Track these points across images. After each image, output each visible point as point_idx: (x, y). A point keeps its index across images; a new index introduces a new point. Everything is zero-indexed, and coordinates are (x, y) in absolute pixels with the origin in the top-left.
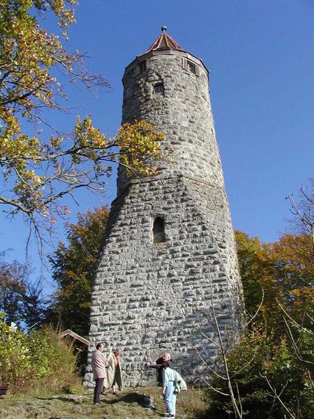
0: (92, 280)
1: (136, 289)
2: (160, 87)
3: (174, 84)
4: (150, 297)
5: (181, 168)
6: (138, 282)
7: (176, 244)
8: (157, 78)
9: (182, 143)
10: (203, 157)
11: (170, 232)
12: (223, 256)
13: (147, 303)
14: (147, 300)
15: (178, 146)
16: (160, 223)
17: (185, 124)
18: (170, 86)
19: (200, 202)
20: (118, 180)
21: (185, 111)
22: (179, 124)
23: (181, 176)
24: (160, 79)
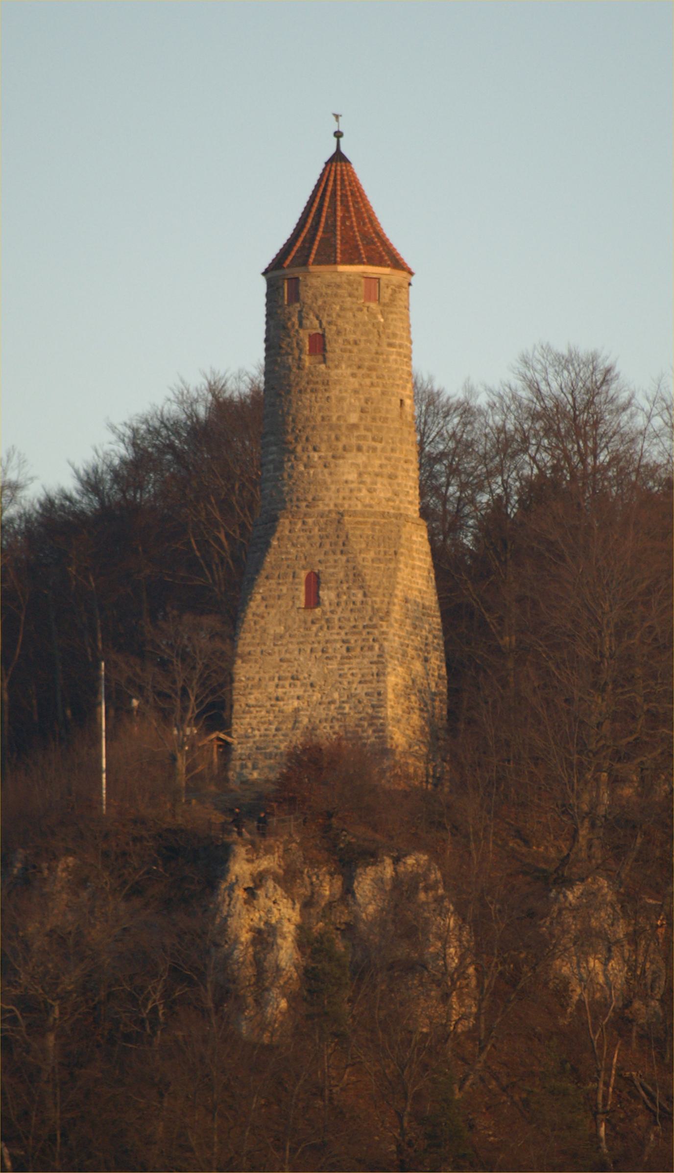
1: (285, 665)
2: (319, 345)
4: (301, 677)
6: (288, 656)
7: (332, 612)
8: (316, 322)
11: (327, 595)
12: (383, 633)
13: (298, 683)
14: (298, 679)
16: (314, 582)
17: (353, 418)
18: (335, 346)
23: (342, 515)
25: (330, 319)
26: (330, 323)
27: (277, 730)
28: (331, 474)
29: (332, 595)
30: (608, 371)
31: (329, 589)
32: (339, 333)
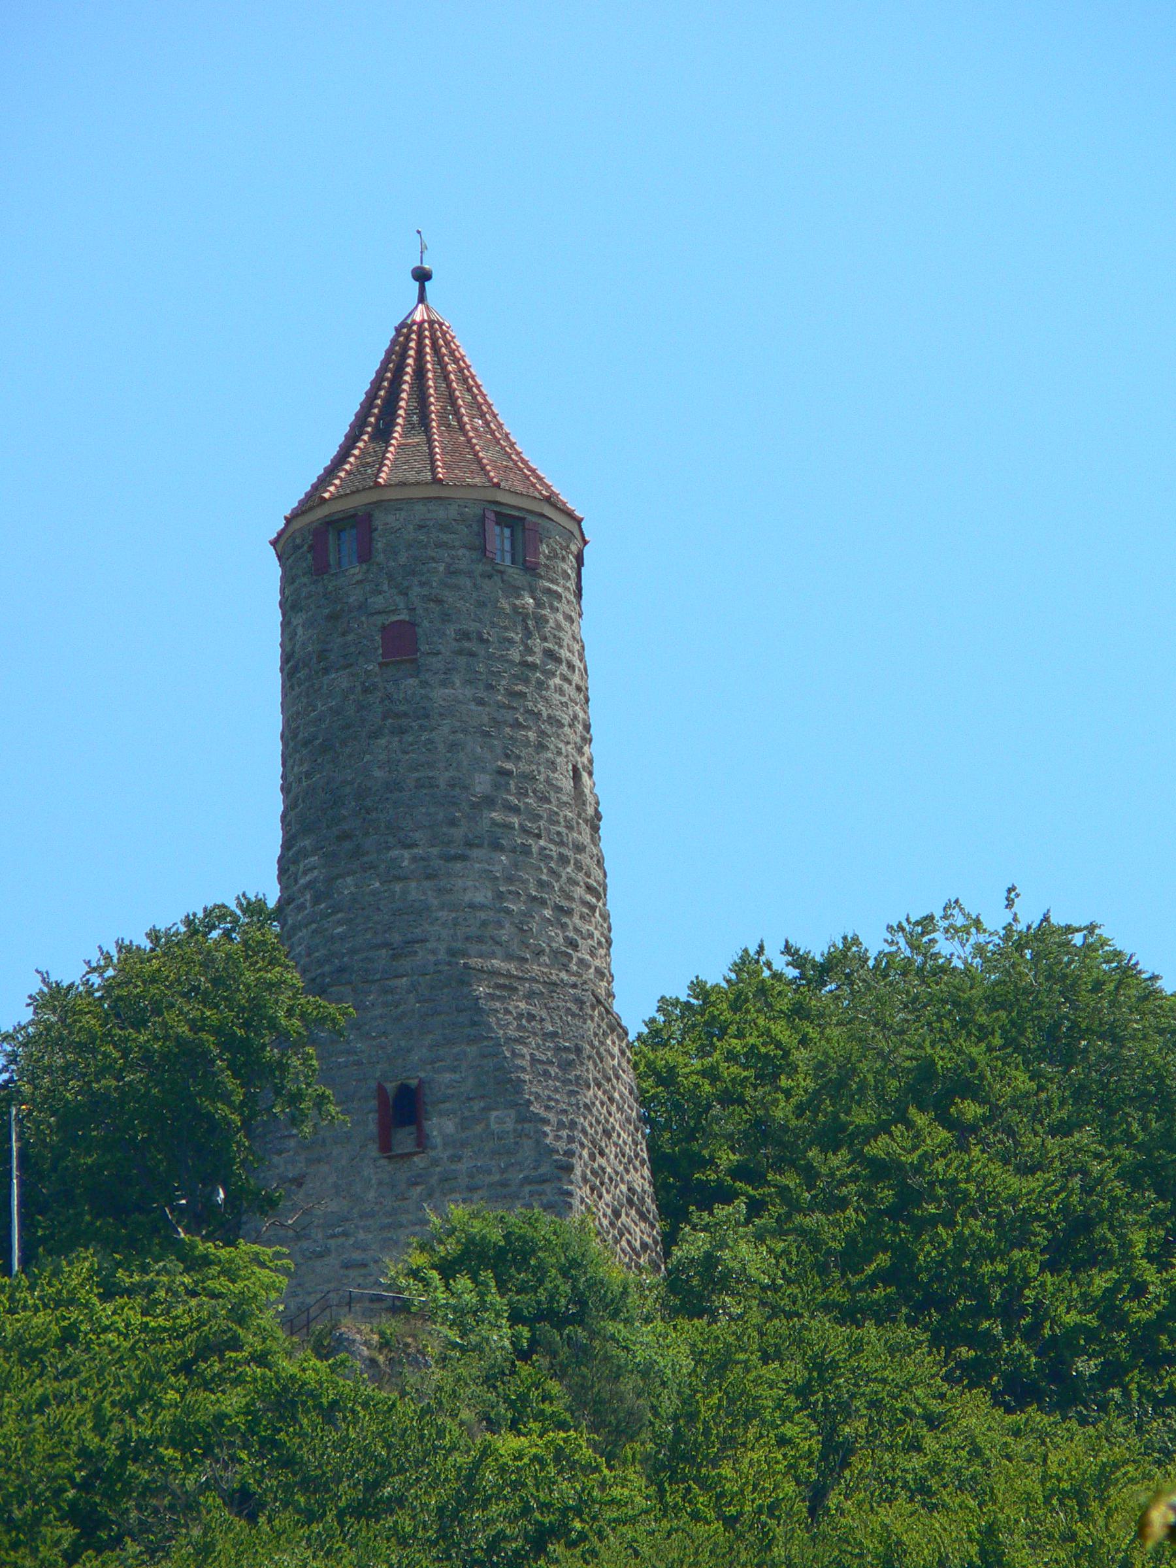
1: (352, 1273)
3: (450, 630)
5: (467, 939)
6: (357, 1256)
9: (475, 853)
15: (459, 866)
25: (425, 591)
26: (428, 599)
27: (460, 1011)
28: (440, 891)
29: (450, 1126)
30: (890, 928)
31: (441, 1114)
32: (446, 617)
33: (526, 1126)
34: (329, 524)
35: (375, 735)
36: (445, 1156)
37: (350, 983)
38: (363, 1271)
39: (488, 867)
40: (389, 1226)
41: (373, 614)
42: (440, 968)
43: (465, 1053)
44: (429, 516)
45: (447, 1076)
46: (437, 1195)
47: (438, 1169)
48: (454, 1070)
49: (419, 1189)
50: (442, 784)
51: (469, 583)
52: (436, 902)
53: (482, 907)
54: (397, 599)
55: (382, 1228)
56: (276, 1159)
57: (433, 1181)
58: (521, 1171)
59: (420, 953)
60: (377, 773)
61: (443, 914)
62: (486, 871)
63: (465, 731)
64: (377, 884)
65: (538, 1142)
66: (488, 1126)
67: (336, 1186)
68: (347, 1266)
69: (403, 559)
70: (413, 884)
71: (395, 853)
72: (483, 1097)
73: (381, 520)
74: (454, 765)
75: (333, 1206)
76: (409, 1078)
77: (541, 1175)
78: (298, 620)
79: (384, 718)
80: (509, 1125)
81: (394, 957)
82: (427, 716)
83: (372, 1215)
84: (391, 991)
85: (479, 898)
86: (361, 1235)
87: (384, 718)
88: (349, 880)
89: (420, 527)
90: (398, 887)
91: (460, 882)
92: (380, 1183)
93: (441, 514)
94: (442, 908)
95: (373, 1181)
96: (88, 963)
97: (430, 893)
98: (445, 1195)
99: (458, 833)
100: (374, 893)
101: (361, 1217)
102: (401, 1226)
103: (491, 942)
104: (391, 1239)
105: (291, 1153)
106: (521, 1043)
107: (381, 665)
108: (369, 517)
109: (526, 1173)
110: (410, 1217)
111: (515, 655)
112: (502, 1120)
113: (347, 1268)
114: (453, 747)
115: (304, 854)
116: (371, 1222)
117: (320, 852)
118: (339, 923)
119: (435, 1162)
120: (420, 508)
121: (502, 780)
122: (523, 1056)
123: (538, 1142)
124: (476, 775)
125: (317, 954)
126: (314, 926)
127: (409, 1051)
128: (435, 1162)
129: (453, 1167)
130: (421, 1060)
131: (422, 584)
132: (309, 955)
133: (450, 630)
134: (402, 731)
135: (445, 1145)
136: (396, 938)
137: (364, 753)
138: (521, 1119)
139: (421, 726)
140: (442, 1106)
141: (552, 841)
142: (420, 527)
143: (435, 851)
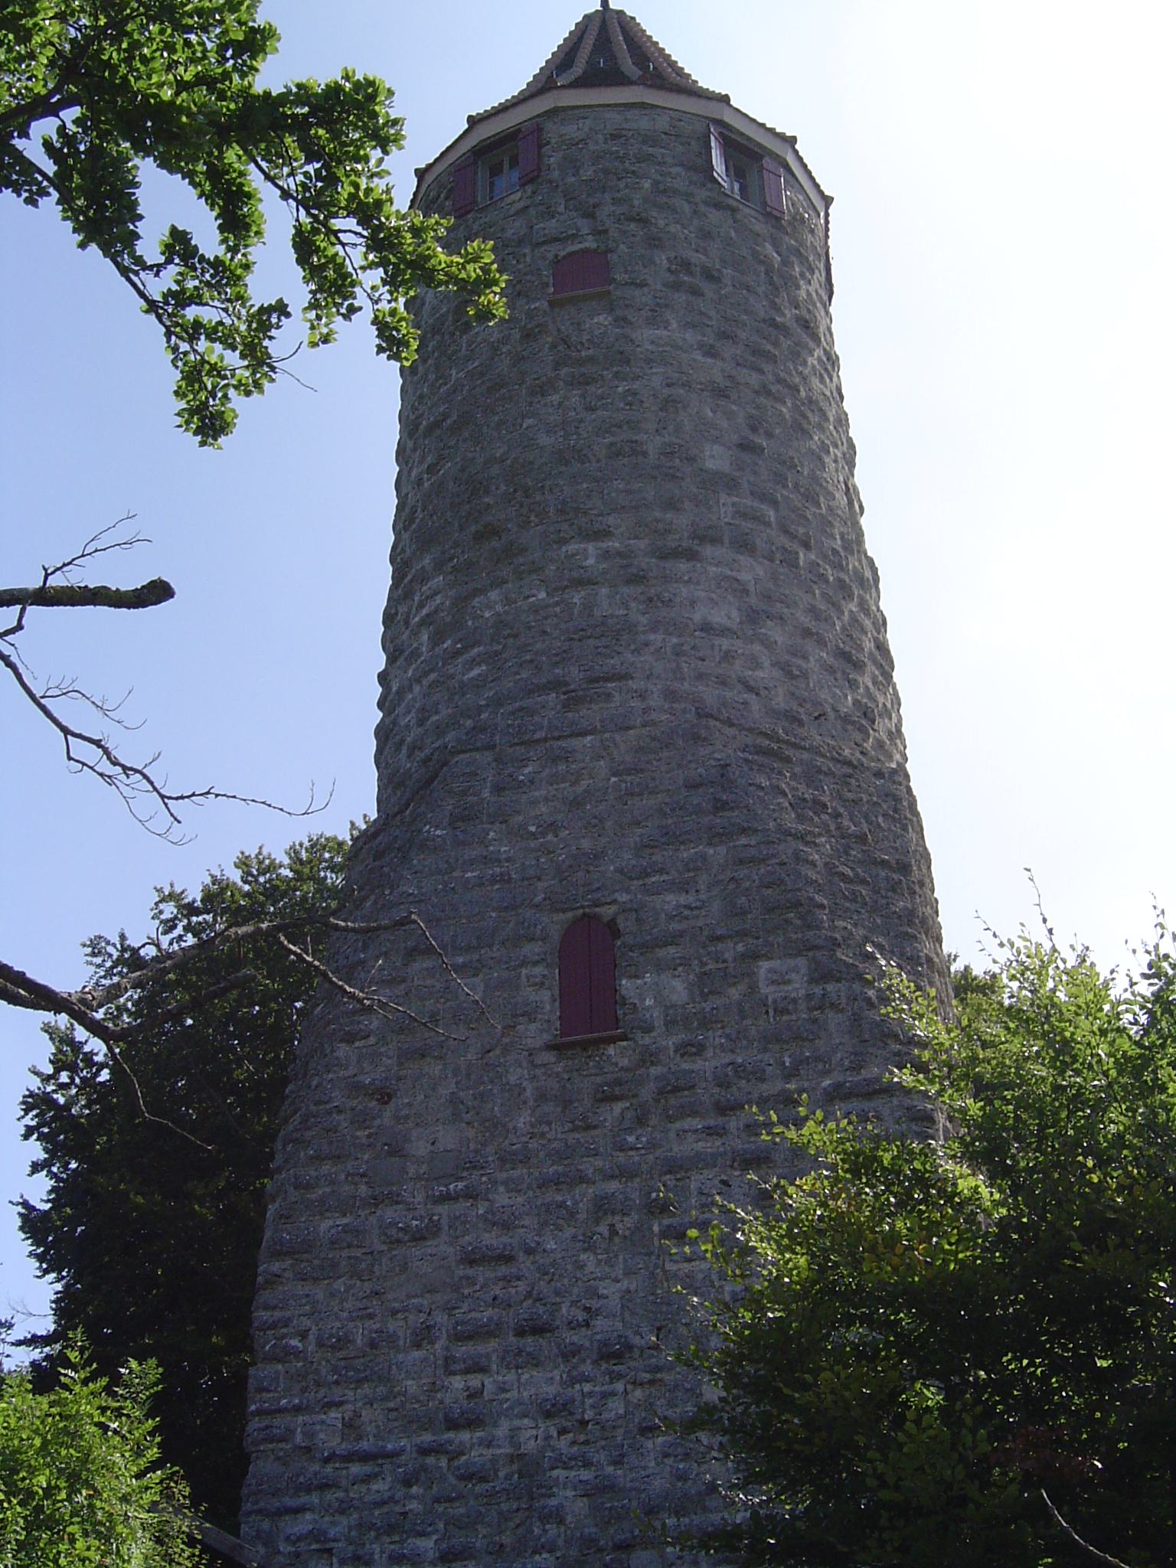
0: (242, 1340)
1: (481, 1273)
3: (662, 259)
5: (700, 676)
6: (491, 1239)
9: (708, 551)
10: (806, 620)
11: (652, 991)
15: (683, 566)
17: (716, 458)
19: (794, 844)
20: (383, 733)
21: (721, 393)
22: (691, 460)
24: (600, 233)
29: (678, 989)
32: (655, 242)
33: (830, 987)
34: (481, 151)
35: (542, 390)
36: (671, 1042)
37: (491, 747)
38: (503, 1270)
39: (729, 573)
40: (556, 1182)
41: (539, 245)
42: (654, 716)
43: (704, 857)
44: (625, 126)
45: (672, 900)
46: (654, 1120)
47: (654, 1071)
48: (683, 887)
49: (618, 1107)
50: (652, 449)
51: (687, 208)
52: (643, 620)
53: (724, 632)
54: (581, 222)
55: (544, 1184)
56: (343, 1050)
57: (647, 1092)
58: (826, 1073)
59: (617, 698)
60: (544, 440)
61: (655, 638)
62: (727, 578)
63: (688, 385)
64: (542, 595)
65: (857, 1019)
66: (753, 988)
67: (454, 1100)
68: (471, 1259)
69: (587, 173)
70: (604, 591)
71: (572, 547)
72: (742, 934)
73: (553, 132)
74: (671, 428)
75: (448, 1138)
76: (597, 904)
77: (868, 1082)
78: (405, 536)
79: (557, 365)
80: (798, 987)
81: (567, 706)
82: (628, 362)
83: (524, 1158)
84: (567, 756)
85: (718, 617)
86: (502, 1198)
87: (557, 365)
88: (494, 595)
89: (614, 137)
90: (577, 598)
91: (684, 591)
92: (542, 1097)
93: (644, 123)
94: (654, 629)
95: (528, 1093)
96: (159, 891)
97: (633, 605)
98: (671, 1119)
99: (682, 521)
100: (535, 610)
101: (502, 1160)
102: (583, 1179)
103: (740, 687)
104: (561, 1205)
105: (372, 1040)
106: (807, 843)
107: (552, 304)
108: (539, 129)
109: (837, 1077)
110: (599, 1163)
111: (760, 308)
112: (781, 977)
113: (472, 1262)
114: (668, 404)
115: (423, 578)
116: (520, 1172)
117: (448, 567)
118: (473, 663)
119: (649, 1057)
120: (615, 117)
121: (747, 458)
122: (813, 864)
123: (857, 1019)
124: (707, 447)
125: (435, 718)
126: (433, 676)
127: (598, 856)
128: (649, 1057)
129: (685, 1066)
130: (620, 871)
131: (616, 201)
132: (421, 723)
133: (662, 259)
134: (585, 381)
135: (670, 1023)
136: (575, 674)
137: (523, 417)
138: (822, 975)
139: (616, 375)
140: (661, 953)
141: (825, 557)
142: (614, 137)
143: (642, 544)
